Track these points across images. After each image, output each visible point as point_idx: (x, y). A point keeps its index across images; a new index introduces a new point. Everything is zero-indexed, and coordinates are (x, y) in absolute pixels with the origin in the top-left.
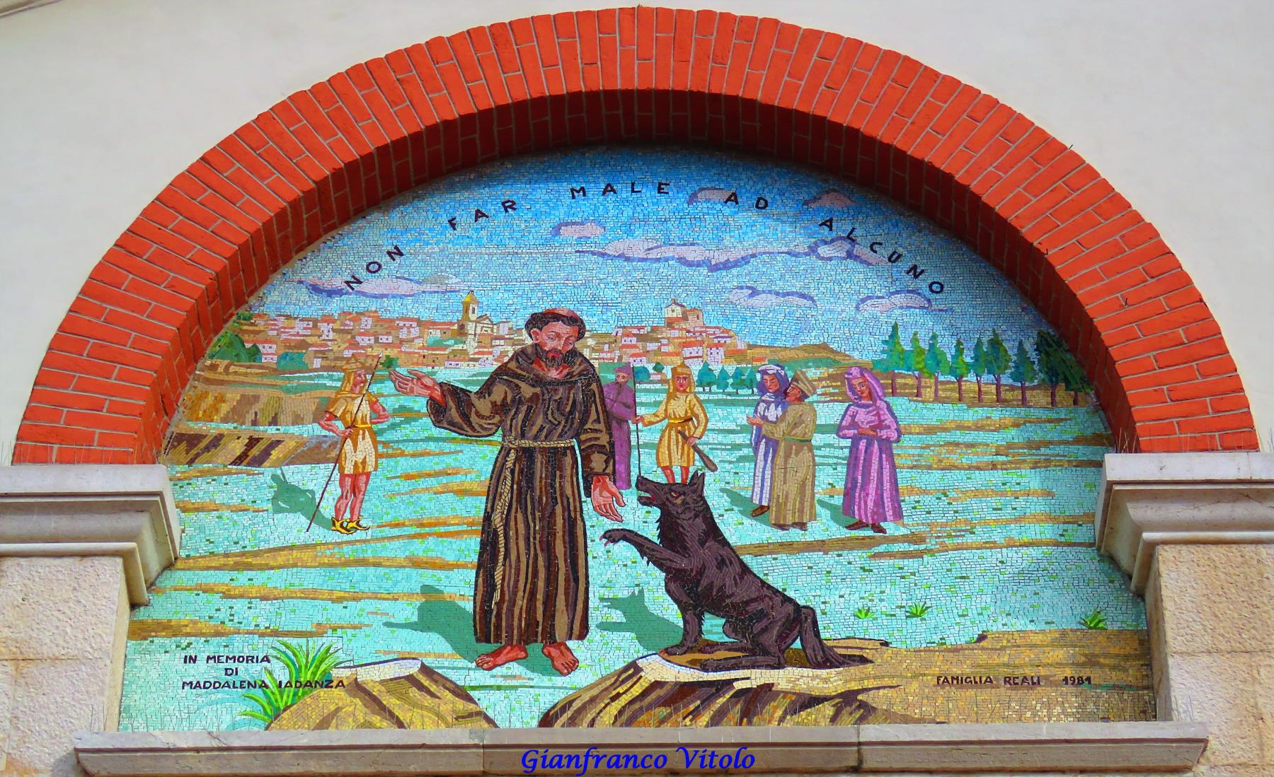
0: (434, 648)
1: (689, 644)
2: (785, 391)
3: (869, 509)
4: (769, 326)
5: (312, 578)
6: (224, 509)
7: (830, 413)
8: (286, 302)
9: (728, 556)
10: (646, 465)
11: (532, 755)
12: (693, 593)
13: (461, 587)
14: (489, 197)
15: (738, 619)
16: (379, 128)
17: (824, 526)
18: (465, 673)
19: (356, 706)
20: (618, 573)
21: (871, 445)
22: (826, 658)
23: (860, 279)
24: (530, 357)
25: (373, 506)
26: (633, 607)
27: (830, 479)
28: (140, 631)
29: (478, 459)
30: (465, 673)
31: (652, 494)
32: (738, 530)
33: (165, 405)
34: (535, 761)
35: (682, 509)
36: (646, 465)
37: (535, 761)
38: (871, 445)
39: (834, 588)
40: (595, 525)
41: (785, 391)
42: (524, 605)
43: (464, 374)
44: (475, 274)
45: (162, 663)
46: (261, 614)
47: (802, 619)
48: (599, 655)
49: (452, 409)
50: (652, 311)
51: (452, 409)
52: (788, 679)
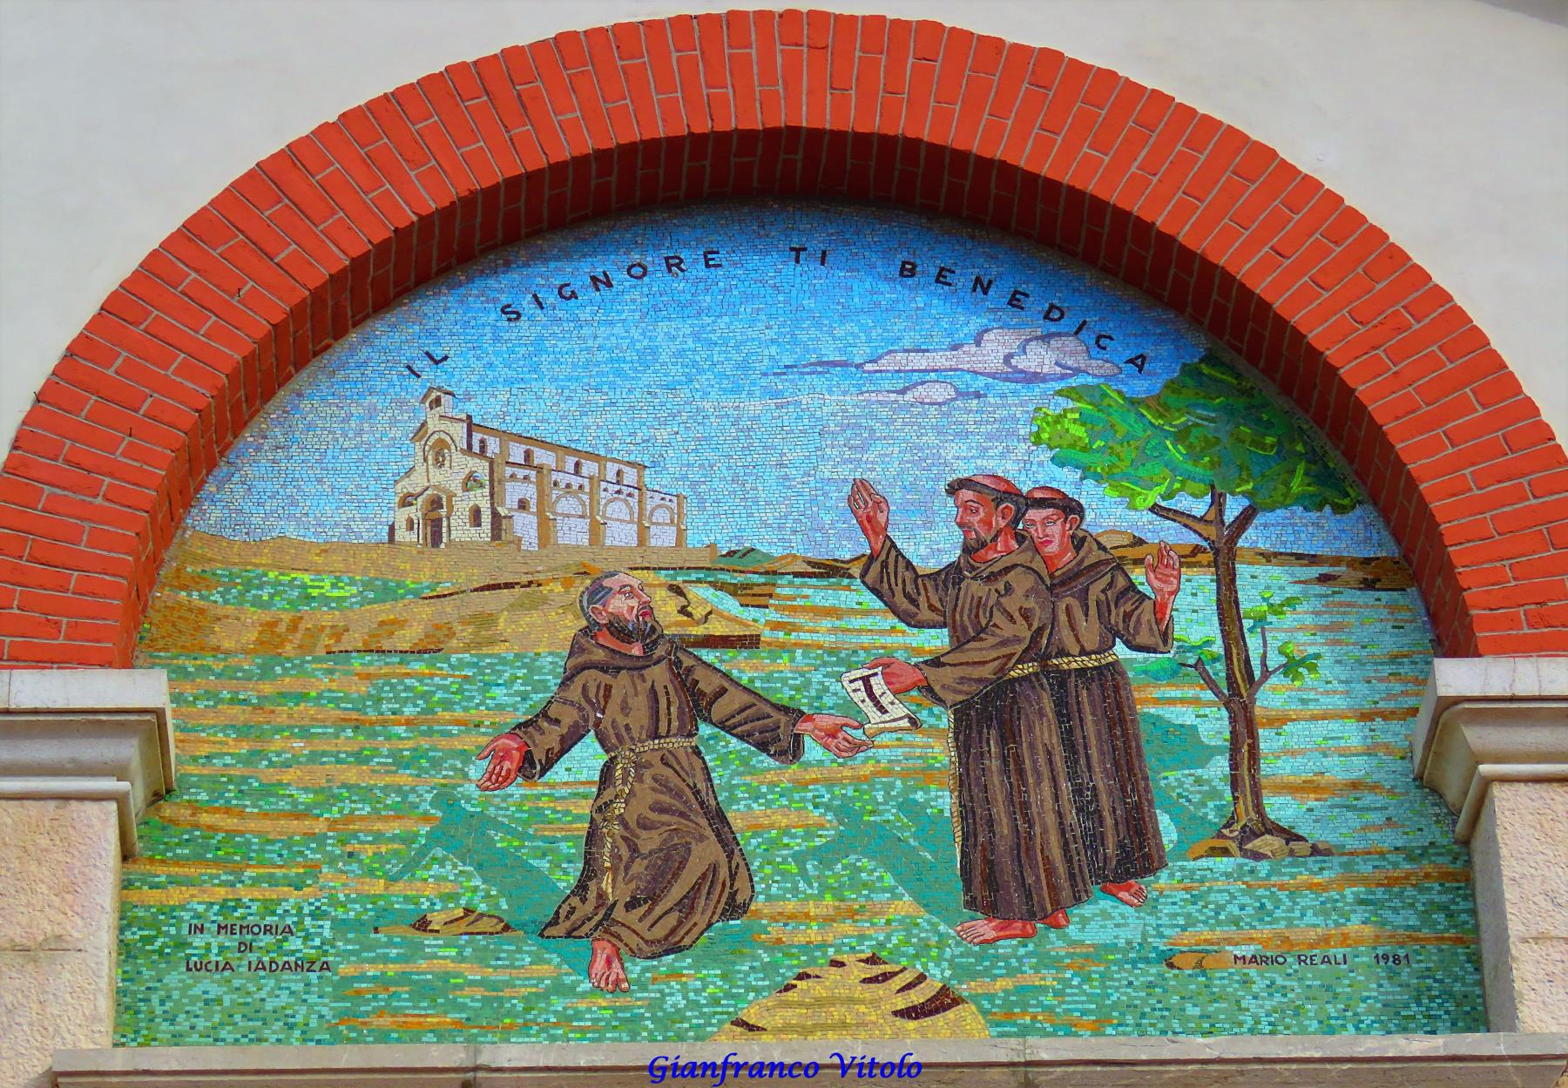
11: (661, 1062)
16: (572, 132)
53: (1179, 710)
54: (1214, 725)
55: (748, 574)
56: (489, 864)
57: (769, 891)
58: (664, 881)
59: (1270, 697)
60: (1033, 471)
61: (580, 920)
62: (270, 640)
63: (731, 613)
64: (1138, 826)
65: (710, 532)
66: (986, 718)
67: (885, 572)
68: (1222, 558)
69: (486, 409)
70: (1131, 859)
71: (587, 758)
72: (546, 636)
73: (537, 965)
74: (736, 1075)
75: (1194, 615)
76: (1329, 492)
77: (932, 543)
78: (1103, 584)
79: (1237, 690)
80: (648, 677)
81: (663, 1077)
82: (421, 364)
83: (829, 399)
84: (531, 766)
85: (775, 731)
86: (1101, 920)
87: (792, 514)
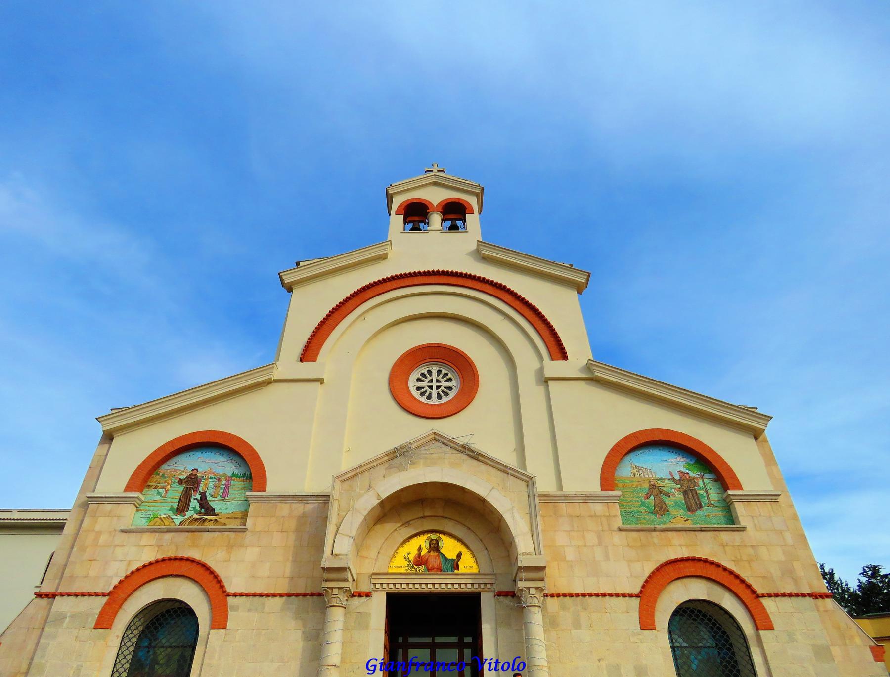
0: (170, 513)
1: (199, 513)
2: (219, 480)
3: (224, 496)
4: (219, 471)
5: (158, 504)
6: (151, 494)
7: (223, 483)
8: (165, 468)
9: (207, 502)
10: (201, 490)
11: (373, 662)
12: (201, 506)
13: (175, 505)
14: (191, 453)
15: (206, 510)
17: (219, 498)
18: (173, 516)
19: (160, 521)
20: (194, 504)
21: (227, 487)
22: (214, 515)
23: (231, 465)
24: (191, 475)
25: (168, 494)
26: (194, 508)
27: (221, 492)
28: (137, 511)
29: (181, 488)
30: (173, 516)
31: (201, 493)
32: (209, 498)
33: (146, 482)
34: (375, 666)
35: (203, 495)
36: (201, 490)
37: (375, 666)
38: (227, 487)
39: (218, 506)
40: (193, 497)
41: (219, 480)
42: (181, 509)
43: (182, 477)
44: (186, 464)
45: (139, 515)
46: (151, 509)
47: (213, 510)
48: (189, 514)
49: (180, 482)
50: (207, 469)
51: (180, 482)
52: (210, 518)
53: (702, 493)
54: (705, 494)
55: (661, 480)
56: (646, 507)
57: (671, 510)
58: (661, 509)
59: (709, 491)
60: (685, 470)
61: (654, 513)
62: (623, 486)
63: (661, 484)
64: (700, 504)
65: (658, 476)
66: (685, 493)
67: (674, 479)
68: (702, 478)
69: (637, 464)
70: (701, 507)
71: (652, 497)
72: (646, 486)
73: (652, 517)
74: (417, 670)
75: (701, 484)
76: (710, 473)
77: (677, 477)
78: (691, 480)
79: (706, 491)
80: (655, 489)
81: (374, 670)
82: (438, 384)
83: (665, 463)
84: (648, 498)
85: (668, 495)
86: (699, 513)
87: (664, 475)
